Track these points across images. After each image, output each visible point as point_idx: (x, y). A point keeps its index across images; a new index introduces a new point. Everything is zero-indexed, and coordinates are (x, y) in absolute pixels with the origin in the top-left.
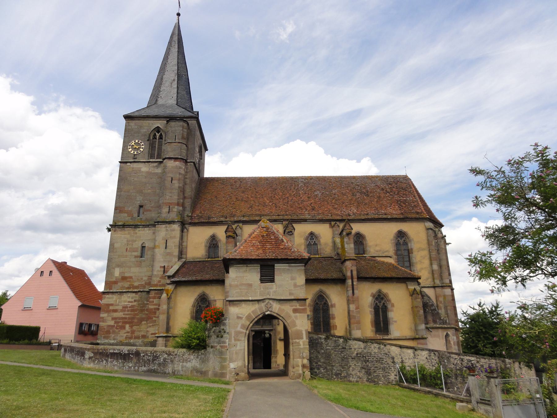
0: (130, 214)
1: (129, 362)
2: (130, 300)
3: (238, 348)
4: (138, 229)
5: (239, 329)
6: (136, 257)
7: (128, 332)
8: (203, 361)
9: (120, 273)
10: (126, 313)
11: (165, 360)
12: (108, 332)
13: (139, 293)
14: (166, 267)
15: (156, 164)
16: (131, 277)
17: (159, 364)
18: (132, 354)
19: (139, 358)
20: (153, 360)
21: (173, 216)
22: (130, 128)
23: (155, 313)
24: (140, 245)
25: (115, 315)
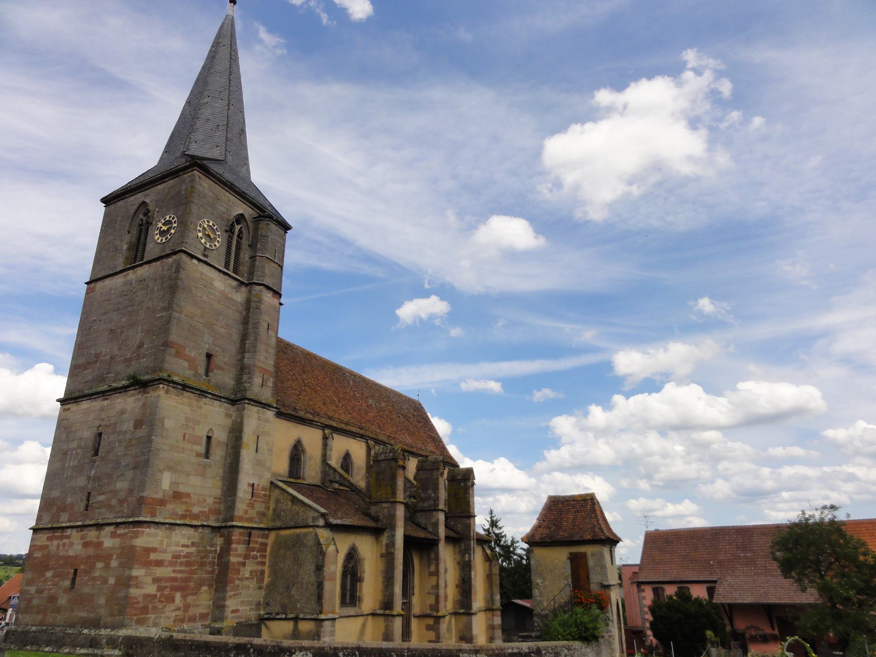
4: (204, 400)
6: (198, 455)
7: (178, 609)
10: (178, 568)
12: (145, 610)
13: (200, 530)
16: (188, 495)
22: (202, 190)
25: (160, 572)
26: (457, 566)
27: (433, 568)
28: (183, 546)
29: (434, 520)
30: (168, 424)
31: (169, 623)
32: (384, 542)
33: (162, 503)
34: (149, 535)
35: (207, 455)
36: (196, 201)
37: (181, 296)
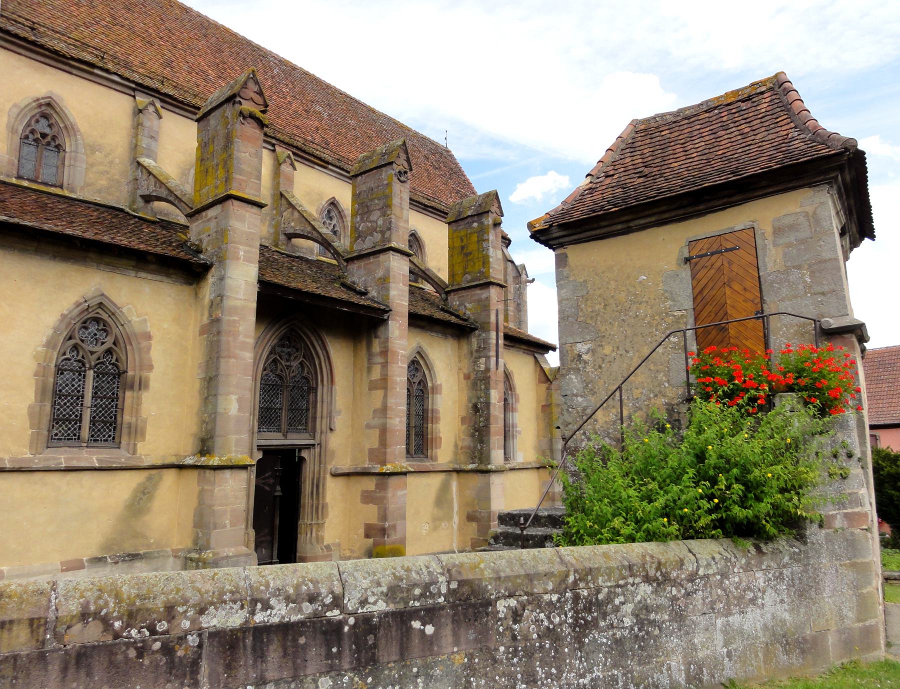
8: (804, 591)
11: (643, 612)
18: (430, 614)
19: (484, 633)
20: (581, 628)
26: (464, 382)
27: (376, 374)
29: (380, 273)
32: (207, 301)
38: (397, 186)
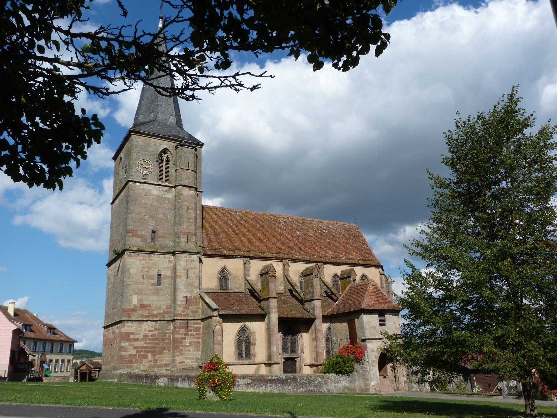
0: (143, 238)
1: (287, 386)
2: (150, 328)
3: (374, 371)
4: (153, 256)
5: (373, 359)
6: (153, 285)
7: (151, 361)
9: (138, 301)
10: (147, 342)
11: (319, 382)
12: (130, 362)
13: (159, 322)
14: (188, 297)
15: (167, 188)
16: (150, 306)
17: (315, 386)
18: (290, 379)
20: (309, 383)
21: (191, 247)
22: (137, 143)
23: (181, 342)
24: (156, 273)
25: (137, 344)
28: (149, 331)
30: (132, 271)
31: (146, 368)
33: (134, 310)
34: (129, 326)
35: (159, 283)
36: (134, 151)
37: (132, 206)
38: (315, 280)
